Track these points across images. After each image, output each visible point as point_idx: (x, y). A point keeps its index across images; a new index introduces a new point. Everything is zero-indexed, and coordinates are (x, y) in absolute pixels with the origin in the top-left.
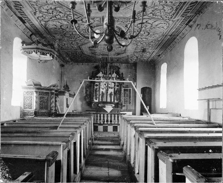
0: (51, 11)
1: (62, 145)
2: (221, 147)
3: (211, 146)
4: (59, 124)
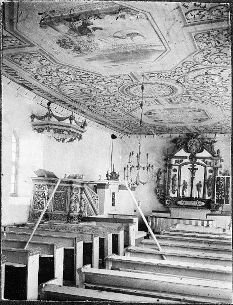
3: (82, 260)
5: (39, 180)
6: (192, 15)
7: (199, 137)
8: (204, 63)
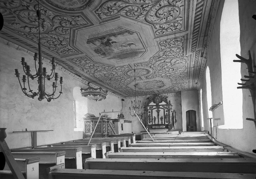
2: (40, 165)
5: (86, 119)
6: (158, 32)
7: (160, 95)
8: (163, 56)
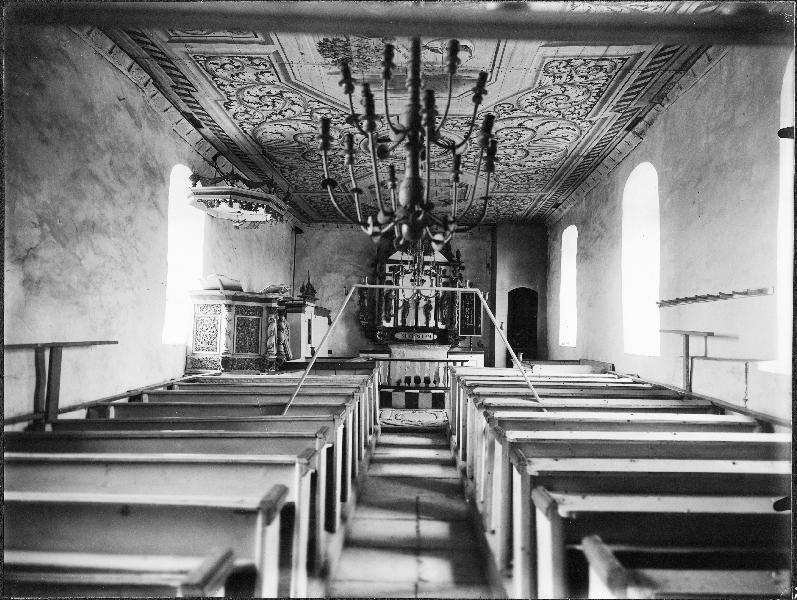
0: (268, 100)
1: (297, 465)
4: (290, 395)
